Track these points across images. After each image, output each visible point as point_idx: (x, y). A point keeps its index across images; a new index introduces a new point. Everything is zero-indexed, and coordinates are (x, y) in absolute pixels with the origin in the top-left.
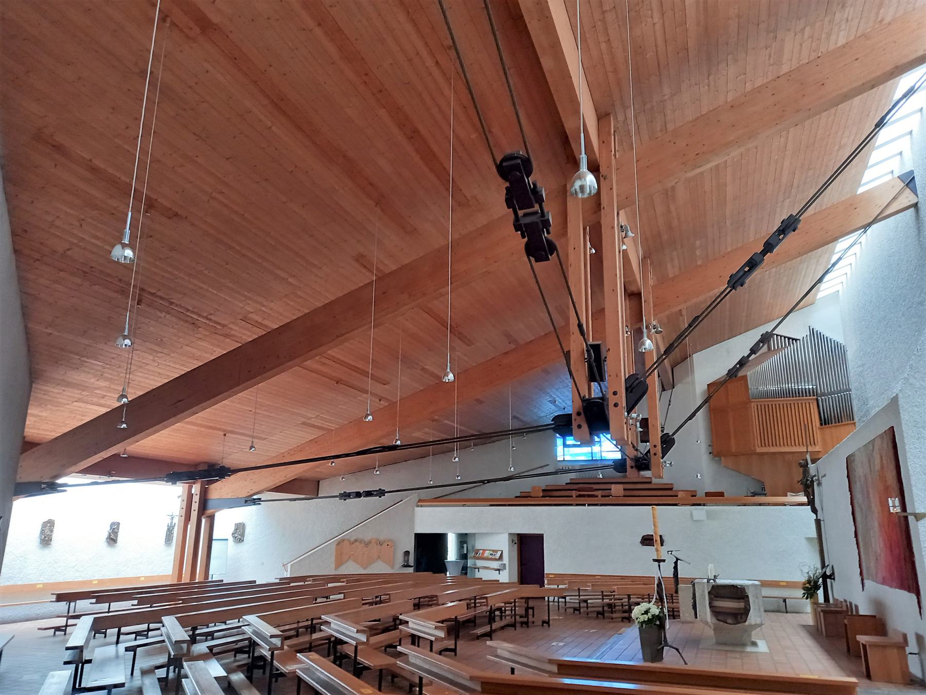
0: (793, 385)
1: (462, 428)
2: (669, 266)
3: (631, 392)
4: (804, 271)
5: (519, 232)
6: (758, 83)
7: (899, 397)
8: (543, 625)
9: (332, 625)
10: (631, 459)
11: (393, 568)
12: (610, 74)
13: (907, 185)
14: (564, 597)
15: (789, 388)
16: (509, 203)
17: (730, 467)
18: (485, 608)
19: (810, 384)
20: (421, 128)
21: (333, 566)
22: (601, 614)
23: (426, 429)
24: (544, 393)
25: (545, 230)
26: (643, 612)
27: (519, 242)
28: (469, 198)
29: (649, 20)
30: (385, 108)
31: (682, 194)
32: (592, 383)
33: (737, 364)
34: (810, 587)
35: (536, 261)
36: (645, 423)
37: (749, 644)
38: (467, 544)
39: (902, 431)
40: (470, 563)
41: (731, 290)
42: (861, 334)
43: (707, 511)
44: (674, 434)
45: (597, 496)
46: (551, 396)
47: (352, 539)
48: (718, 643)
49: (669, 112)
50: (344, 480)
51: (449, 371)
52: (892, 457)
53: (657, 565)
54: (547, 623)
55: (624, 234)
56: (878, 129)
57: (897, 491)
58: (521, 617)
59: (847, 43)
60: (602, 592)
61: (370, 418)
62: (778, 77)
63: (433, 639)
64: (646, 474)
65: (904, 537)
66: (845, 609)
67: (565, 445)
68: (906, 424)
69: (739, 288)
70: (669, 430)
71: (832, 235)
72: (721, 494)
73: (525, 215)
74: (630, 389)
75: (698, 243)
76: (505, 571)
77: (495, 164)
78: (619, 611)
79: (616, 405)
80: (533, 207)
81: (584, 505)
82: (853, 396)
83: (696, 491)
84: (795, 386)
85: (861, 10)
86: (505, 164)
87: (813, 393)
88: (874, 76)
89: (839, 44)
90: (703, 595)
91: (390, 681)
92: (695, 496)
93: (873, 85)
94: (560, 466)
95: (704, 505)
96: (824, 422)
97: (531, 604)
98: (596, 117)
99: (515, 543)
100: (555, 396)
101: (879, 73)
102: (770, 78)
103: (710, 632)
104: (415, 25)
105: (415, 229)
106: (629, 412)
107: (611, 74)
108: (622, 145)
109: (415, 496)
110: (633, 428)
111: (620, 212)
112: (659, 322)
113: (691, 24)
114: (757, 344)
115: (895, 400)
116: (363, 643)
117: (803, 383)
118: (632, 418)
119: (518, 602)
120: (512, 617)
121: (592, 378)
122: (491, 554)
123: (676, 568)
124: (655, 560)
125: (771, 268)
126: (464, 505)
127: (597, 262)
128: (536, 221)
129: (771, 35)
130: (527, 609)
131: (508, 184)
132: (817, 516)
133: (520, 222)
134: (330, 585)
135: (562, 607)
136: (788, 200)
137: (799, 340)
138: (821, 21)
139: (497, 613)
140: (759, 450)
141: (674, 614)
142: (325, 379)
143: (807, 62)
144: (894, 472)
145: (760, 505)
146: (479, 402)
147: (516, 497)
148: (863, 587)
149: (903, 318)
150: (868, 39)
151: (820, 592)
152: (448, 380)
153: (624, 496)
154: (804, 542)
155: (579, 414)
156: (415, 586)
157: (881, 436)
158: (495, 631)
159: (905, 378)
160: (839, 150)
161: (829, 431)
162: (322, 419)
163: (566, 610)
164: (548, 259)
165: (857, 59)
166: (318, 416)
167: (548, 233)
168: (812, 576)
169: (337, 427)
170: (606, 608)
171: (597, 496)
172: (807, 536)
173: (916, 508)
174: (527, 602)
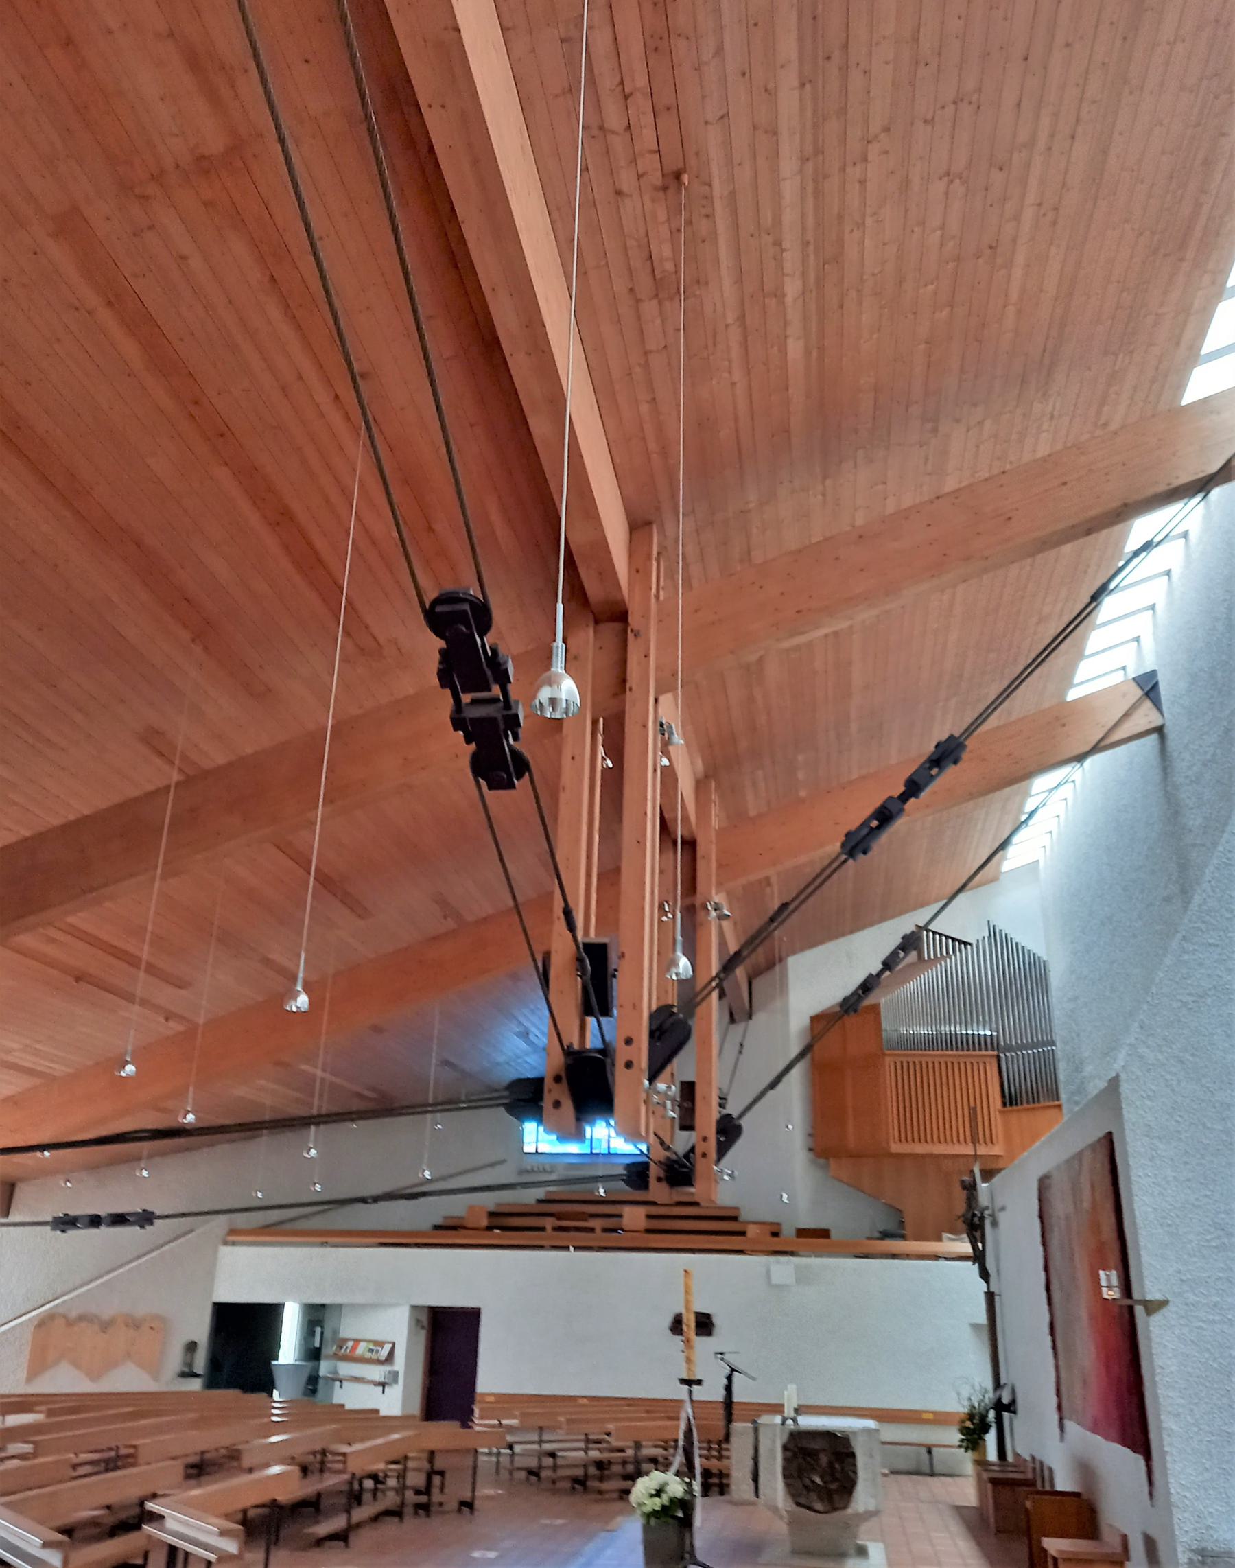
0: (958, 1028)
1: (338, 1081)
2: (750, 797)
3: (659, 1039)
6: (907, 502)
7: (1120, 1078)
8: (460, 1511)
12: (655, 457)
15: (950, 1033)
16: (445, 677)
17: (845, 1180)
19: (987, 1026)
21: (23, 1374)
22: (580, 1483)
25: (509, 732)
26: (654, 1492)
27: (460, 748)
28: (382, 640)
29: (726, 375)
31: (773, 672)
34: (972, 1426)
35: (490, 788)
36: (688, 1090)
37: (852, 1551)
38: (322, 1327)
39: (1124, 1143)
40: (324, 1368)
42: (1073, 942)
43: (797, 1267)
46: (520, 1023)
47: (74, 1314)
48: (796, 1552)
49: (755, 530)
51: (299, 988)
52: (1110, 1188)
54: (467, 1505)
58: (418, 1492)
61: (130, 1069)
62: (938, 498)
63: (212, 1557)
68: (1132, 1130)
70: (733, 1109)
72: (824, 1233)
73: (475, 702)
74: (657, 1034)
75: (800, 758)
76: (395, 1386)
79: (629, 1065)
81: (567, 1248)
82: (1059, 1054)
83: (778, 1224)
84: (961, 1030)
86: (439, 609)
87: (990, 1043)
88: (1093, 513)
89: (1040, 454)
90: (772, 1452)
95: (792, 1254)
96: (1010, 1100)
97: (439, 1465)
98: (626, 522)
103: (782, 1527)
104: (299, 328)
105: (270, 690)
106: (652, 1079)
107: (655, 455)
109: (222, 1221)
111: (662, 699)
112: (730, 896)
115: (1114, 1083)
117: (975, 1025)
118: (658, 1093)
122: (371, 1350)
126: (324, 1244)
127: (614, 783)
129: (929, 426)
130: (430, 1475)
131: (442, 644)
135: (505, 1468)
137: (970, 944)
138: (1010, 412)
140: (895, 1148)
143: (987, 475)
144: (1113, 1220)
145: (894, 1256)
150: (1082, 453)
151: (991, 1438)
153: (648, 1231)
154: (968, 1331)
155: (557, 1079)
157: (1092, 1147)
158: (359, 1525)
161: (1020, 1118)
164: (512, 786)
165: (1065, 484)
167: (516, 738)
168: (976, 1405)
170: (592, 1471)
173: (1147, 1290)
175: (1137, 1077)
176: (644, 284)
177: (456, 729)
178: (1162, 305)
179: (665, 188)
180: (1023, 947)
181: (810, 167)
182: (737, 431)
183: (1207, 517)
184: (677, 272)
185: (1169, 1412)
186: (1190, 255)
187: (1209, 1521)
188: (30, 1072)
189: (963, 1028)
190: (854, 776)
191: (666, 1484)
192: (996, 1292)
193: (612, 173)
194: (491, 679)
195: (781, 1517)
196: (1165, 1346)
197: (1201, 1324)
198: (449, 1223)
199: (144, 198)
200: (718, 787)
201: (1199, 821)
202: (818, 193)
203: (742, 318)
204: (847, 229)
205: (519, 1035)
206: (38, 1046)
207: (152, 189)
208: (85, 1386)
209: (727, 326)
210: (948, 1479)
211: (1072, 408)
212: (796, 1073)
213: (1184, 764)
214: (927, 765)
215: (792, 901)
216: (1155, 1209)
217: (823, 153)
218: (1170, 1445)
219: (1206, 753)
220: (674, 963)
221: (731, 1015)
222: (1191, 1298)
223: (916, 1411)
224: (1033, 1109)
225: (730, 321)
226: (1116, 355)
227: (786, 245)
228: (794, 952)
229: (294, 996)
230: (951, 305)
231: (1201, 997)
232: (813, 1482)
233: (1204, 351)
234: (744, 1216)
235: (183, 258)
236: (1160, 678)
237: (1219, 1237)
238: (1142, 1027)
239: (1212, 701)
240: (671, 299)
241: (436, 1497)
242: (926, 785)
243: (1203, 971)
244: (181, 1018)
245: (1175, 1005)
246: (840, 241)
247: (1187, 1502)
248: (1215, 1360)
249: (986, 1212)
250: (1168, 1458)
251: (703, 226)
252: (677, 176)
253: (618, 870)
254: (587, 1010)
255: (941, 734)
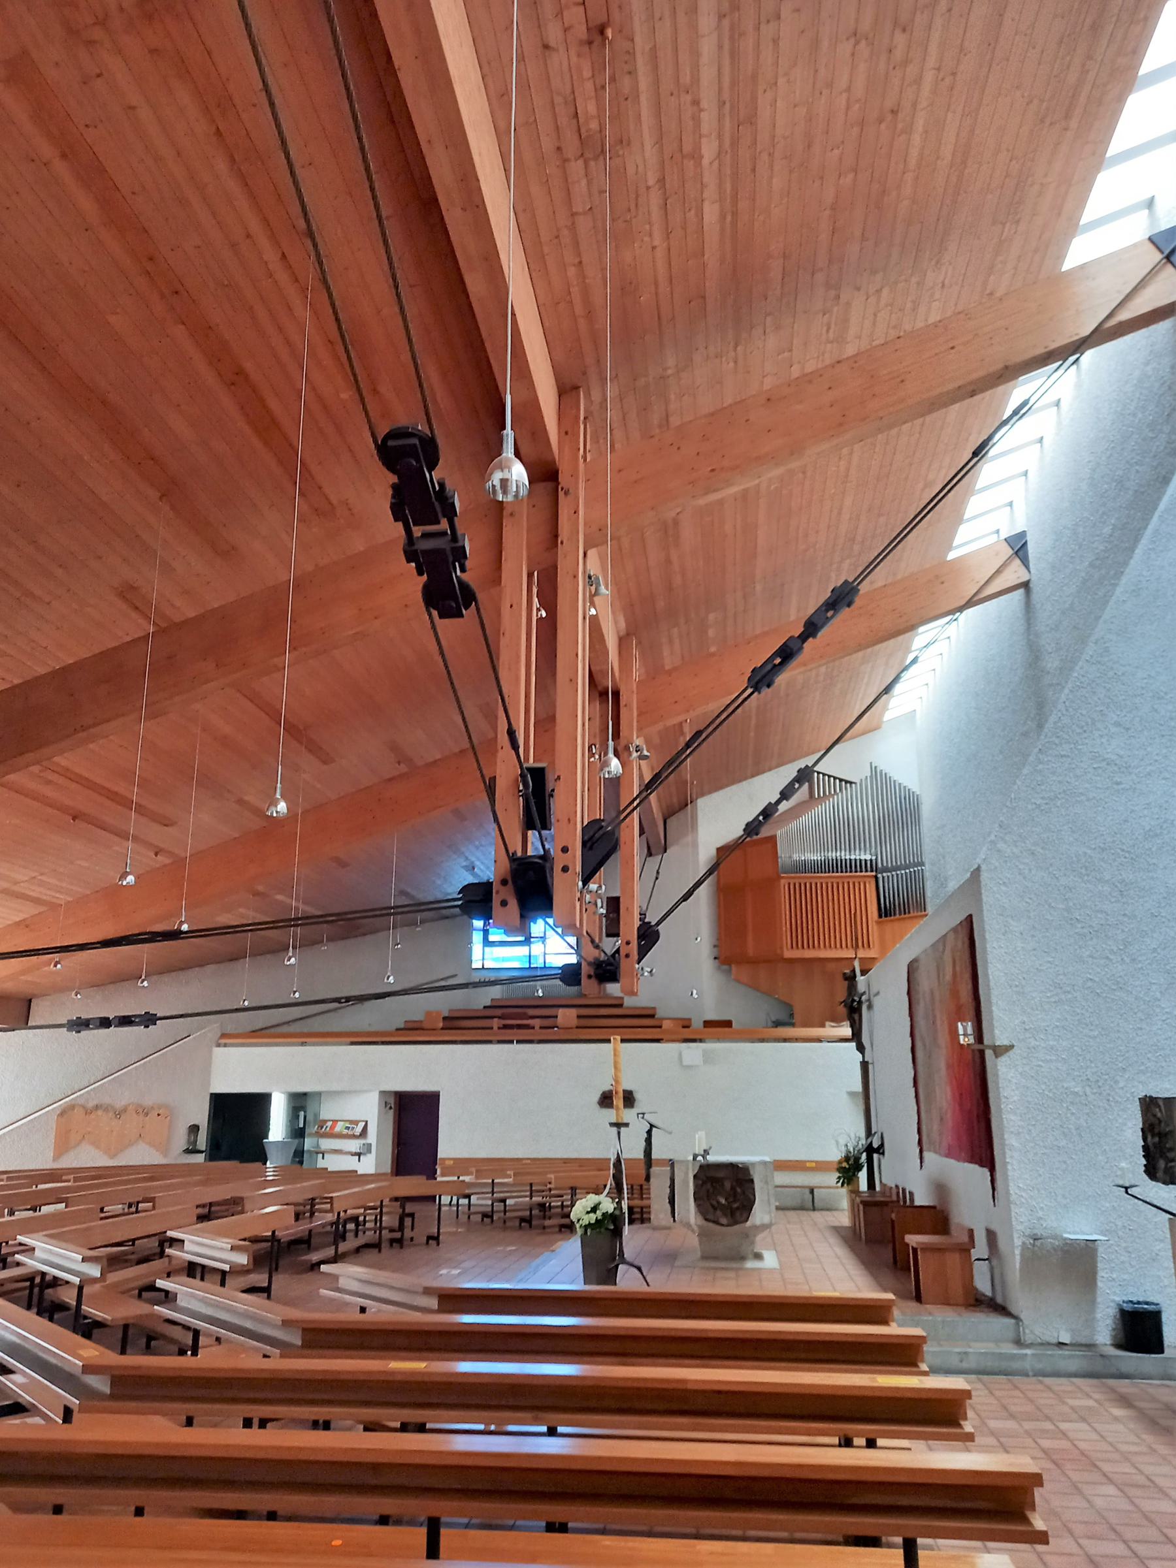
2: (666, 652)
4: (866, 676)
5: (413, 564)
6: (810, 367)
9: (37, 1253)
10: (589, 964)
11: (165, 1156)
13: (1016, 553)
14: (468, 1196)
16: (398, 512)
18: (330, 1217)
19: (868, 852)
20: (249, 366)
22: (526, 1222)
23: (241, 910)
24: (455, 853)
27: (413, 583)
28: (335, 502)
29: (646, 239)
30: (183, 324)
31: (689, 534)
32: (530, 832)
33: (759, 815)
35: (441, 617)
36: (614, 904)
39: (982, 921)
40: (308, 1144)
41: (752, 693)
44: (658, 923)
45: (533, 1028)
46: (467, 859)
47: (91, 1104)
48: (705, 1258)
49: (672, 397)
50: (79, 996)
51: (278, 796)
53: (616, 1132)
54: (434, 1239)
55: (593, 588)
56: (976, 459)
57: (972, 1013)
58: (392, 1230)
59: (940, 321)
60: (531, 1185)
61: (130, 879)
63: (226, 1267)
64: (613, 989)
65: (978, 1082)
66: (894, 1198)
67: (487, 942)
69: (765, 691)
70: (652, 918)
71: (907, 622)
72: (728, 1024)
73: (425, 536)
75: (712, 617)
76: (368, 1155)
77: (375, 441)
78: (556, 1215)
79: (565, 869)
80: (438, 523)
81: (511, 1042)
82: (927, 874)
85: (963, 272)
86: (391, 443)
87: (872, 866)
88: (975, 376)
89: (931, 320)
90: (686, 1182)
91: (144, 1345)
92: (688, 1027)
93: (974, 391)
94: (476, 977)
95: (701, 1041)
96: (885, 912)
98: (555, 387)
99: (391, 1108)
100: (473, 859)
101: (981, 373)
102: (828, 362)
103: (693, 1241)
106: (586, 882)
108: (598, 442)
109: (214, 1026)
110: (591, 908)
111: (589, 553)
112: (647, 742)
113: (711, 256)
114: (791, 784)
116: (94, 1280)
117: (857, 851)
119: (387, 1206)
120: (375, 1232)
121: (529, 824)
122: (348, 1128)
123: (649, 1141)
124: (612, 1125)
125: (820, 666)
126: (303, 1044)
127: (548, 632)
128: (443, 547)
129: (832, 293)
131: (393, 479)
132: (863, 1057)
133: (416, 547)
134: (41, 1187)
135: (463, 1213)
136: (848, 561)
139: (351, 1226)
140: (788, 954)
141: (639, 1216)
142: (50, 810)
144: (970, 986)
145: (785, 1040)
146: (342, 864)
147: (397, 1029)
148: (921, 1163)
149: (1001, 756)
151: (863, 1175)
152: (277, 812)
153: (577, 1027)
154: (845, 1097)
155: (504, 882)
156: (205, 1183)
157: (955, 930)
159: (992, 842)
160: (923, 490)
161: (891, 926)
162: (42, 884)
163: (469, 1217)
164: (461, 616)
165: (953, 348)
166: (34, 878)
167: (463, 570)
168: (852, 1150)
169: (70, 899)
170: (535, 1212)
171: (533, 1028)
172: (849, 1090)
174: (403, 1207)
175: (996, 868)
176: (571, 146)
177: (409, 561)
178: (1046, 175)
179: (590, 43)
180: (900, 784)
181: (726, 23)
182: (656, 294)
183: (1078, 385)
184: (601, 130)
185: (1012, 1132)
186: (1074, 124)
187: (1040, 1214)
188: (37, 901)
189: (848, 853)
190: (758, 632)
191: (599, 1204)
192: (870, 1061)
193: (539, 26)
194: (440, 515)
195: (693, 1231)
196: (1010, 1081)
197: (1040, 1063)
198: (410, 1025)
199: (91, 43)
200: (639, 643)
201: (1057, 663)
202: (734, 54)
203: (662, 181)
204: (760, 92)
205: (466, 868)
206: (44, 878)
207: (98, 34)
208: (103, 1161)
209: (648, 188)
210: (828, 1212)
211: (961, 278)
212: (703, 891)
213: (1046, 614)
214: (824, 608)
215: (706, 728)
216: (1006, 974)
217: (739, 9)
218: (1012, 1157)
219: (1065, 602)
220: (606, 764)
221: (649, 848)
222: (1033, 1043)
223: (801, 1161)
224: (904, 919)
225: (651, 182)
226: (1004, 224)
227: (704, 104)
228: (703, 795)
229: (274, 803)
230: (855, 171)
231: (1051, 800)
232: (718, 1202)
233: (1084, 221)
234: (660, 1014)
235: (133, 108)
236: (1029, 538)
237: (1057, 994)
238: (1001, 826)
239: (1073, 555)
240: (596, 158)
241: (408, 1233)
242: (822, 627)
243: (1054, 778)
244: (170, 853)
245: (1030, 807)
246: (754, 99)
247: (1023, 1200)
248: (1050, 1091)
249: (864, 998)
250: (1009, 1167)
251: (626, 83)
252: (602, 31)
253: (552, 719)
254: (529, 824)
255: (836, 581)
